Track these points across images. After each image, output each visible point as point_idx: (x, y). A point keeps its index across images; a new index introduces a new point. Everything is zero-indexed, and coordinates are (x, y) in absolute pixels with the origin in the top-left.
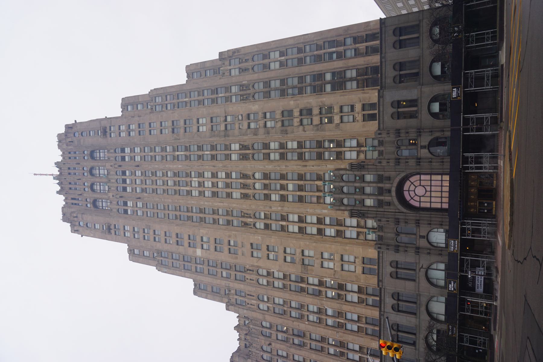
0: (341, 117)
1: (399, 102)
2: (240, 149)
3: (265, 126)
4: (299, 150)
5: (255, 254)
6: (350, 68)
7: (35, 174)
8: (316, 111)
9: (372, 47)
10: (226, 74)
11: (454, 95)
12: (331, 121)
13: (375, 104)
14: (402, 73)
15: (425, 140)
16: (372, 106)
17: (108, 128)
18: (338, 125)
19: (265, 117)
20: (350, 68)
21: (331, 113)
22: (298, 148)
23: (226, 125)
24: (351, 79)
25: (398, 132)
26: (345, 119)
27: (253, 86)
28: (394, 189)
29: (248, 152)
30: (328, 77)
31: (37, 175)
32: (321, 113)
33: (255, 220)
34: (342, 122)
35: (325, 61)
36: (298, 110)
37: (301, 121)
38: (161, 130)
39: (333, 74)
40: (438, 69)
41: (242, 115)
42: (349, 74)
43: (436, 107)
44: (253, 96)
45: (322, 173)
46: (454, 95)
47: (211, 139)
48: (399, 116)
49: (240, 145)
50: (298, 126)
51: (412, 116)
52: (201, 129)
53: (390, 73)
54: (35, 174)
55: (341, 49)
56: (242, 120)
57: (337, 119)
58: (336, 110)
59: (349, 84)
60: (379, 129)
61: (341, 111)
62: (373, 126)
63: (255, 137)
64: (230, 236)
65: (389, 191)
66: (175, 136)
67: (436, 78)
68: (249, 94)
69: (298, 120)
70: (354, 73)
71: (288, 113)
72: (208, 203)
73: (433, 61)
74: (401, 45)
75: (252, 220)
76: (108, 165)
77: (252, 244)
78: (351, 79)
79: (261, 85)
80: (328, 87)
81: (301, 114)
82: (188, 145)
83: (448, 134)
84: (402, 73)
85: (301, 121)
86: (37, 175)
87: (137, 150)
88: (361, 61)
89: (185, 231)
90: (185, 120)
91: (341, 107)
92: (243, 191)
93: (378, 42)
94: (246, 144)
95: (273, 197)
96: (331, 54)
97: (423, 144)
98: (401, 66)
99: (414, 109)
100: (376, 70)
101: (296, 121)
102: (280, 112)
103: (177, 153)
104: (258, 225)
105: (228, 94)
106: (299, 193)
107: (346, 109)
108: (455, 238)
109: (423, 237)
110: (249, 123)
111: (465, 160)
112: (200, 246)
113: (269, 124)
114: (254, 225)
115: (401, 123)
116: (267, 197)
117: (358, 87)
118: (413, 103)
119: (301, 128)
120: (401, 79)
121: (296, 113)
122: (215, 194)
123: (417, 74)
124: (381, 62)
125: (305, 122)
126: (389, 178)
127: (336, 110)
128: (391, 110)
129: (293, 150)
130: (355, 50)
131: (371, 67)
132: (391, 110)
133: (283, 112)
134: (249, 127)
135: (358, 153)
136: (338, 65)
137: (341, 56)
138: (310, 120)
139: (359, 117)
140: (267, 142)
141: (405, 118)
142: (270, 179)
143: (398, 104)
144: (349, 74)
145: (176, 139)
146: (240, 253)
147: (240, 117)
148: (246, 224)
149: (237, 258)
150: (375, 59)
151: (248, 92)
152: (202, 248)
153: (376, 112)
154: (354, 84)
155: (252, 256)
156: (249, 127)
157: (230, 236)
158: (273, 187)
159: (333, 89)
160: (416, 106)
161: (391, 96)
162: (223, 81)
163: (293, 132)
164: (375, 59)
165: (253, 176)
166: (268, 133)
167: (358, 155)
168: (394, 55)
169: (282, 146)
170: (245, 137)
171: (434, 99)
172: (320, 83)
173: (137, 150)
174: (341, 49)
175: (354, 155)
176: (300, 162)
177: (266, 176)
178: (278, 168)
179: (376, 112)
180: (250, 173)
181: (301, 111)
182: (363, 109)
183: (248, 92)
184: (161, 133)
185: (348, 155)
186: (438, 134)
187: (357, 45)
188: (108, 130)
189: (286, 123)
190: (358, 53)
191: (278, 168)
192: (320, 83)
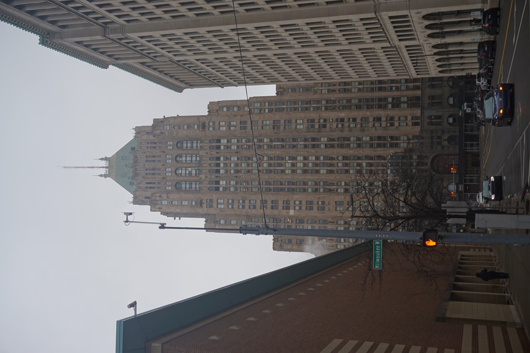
0: (399, 123)
1: (432, 116)
2: (328, 141)
3: (349, 126)
4: (371, 142)
5: (338, 209)
6: (403, 96)
7: (65, 167)
8: (384, 119)
9: (416, 86)
10: (318, 92)
11: (460, 114)
12: (392, 125)
13: (419, 117)
14: (433, 101)
15: (446, 137)
16: (417, 118)
17: (207, 123)
18: (397, 127)
19: (349, 121)
20: (403, 96)
21: (392, 120)
22: (370, 140)
23: (319, 125)
24: (404, 102)
25: (432, 132)
26: (402, 124)
27: (339, 101)
28: (429, 163)
29: (334, 142)
30: (390, 100)
31: (67, 167)
32: (386, 120)
33: (338, 187)
34: (399, 125)
35: (388, 91)
36: (372, 118)
37: (374, 124)
38: (262, 127)
39: (393, 99)
40: (451, 101)
41: (332, 119)
42: (402, 99)
43: (451, 120)
44: (339, 108)
45: (386, 156)
46: (460, 114)
47: (307, 134)
48: (432, 124)
49: (328, 138)
50: (372, 127)
51: (439, 124)
52: (298, 127)
53: (427, 101)
54: (65, 167)
55: (398, 85)
56: (332, 122)
57: (396, 124)
58: (396, 119)
59: (402, 105)
60: (421, 130)
61: (399, 120)
62: (418, 129)
63: (342, 133)
64: (319, 198)
65: (427, 164)
66: (276, 131)
67: (450, 105)
68: (336, 106)
69: (372, 124)
70: (406, 99)
71: (365, 119)
72: (299, 176)
73: (450, 96)
74: (432, 87)
75: (335, 187)
76: (201, 153)
77: (336, 202)
78: (404, 102)
79: (345, 101)
80: (390, 106)
81: (374, 120)
82: (284, 138)
83: (458, 134)
84: (433, 101)
85: (374, 124)
86: (67, 167)
87: (234, 141)
88: (411, 93)
89: (281, 198)
90: (285, 120)
91: (399, 117)
92: (329, 168)
93: (420, 84)
94: (333, 137)
95: (351, 172)
96: (391, 87)
97: (445, 138)
98: (432, 97)
99: (440, 120)
100: (418, 98)
101: (371, 124)
102: (360, 118)
103: (274, 143)
104: (339, 190)
105: (319, 105)
106: (370, 168)
107: (402, 118)
108: (461, 183)
109: (445, 188)
110: (337, 124)
111: (466, 145)
112: (293, 207)
113: (352, 125)
114: (337, 190)
115: (433, 127)
116: (347, 171)
117: (408, 107)
118: (439, 117)
119: (374, 128)
120: (431, 105)
121: (371, 119)
122: (305, 172)
123: (440, 103)
124: (422, 95)
125: (376, 125)
126: (426, 157)
127: (396, 119)
128: (428, 120)
129: (366, 143)
130: (407, 86)
131: (416, 97)
132: (428, 120)
133: (362, 119)
134: (337, 127)
135: (408, 143)
136: (397, 94)
137: (398, 89)
138: (379, 124)
139: (410, 123)
140: (295, 156)
141: (436, 125)
142: (350, 160)
143: (430, 117)
144: (402, 99)
145: (276, 133)
146: (326, 208)
147: (331, 120)
148: (330, 190)
149: (324, 213)
150: (418, 93)
151: (335, 105)
152: (295, 209)
153: (420, 121)
154: (406, 105)
155: (336, 210)
156: (337, 127)
157: (319, 198)
158: (351, 165)
159: (393, 107)
160: (441, 119)
161: (427, 113)
162: (316, 97)
163: (368, 131)
164: (418, 93)
165: (337, 158)
166: (351, 131)
167: (408, 145)
168: (429, 92)
169: (359, 139)
170: (334, 133)
171: (450, 116)
172: (385, 103)
173: (234, 141)
174: (398, 85)
175: (405, 145)
176: (371, 149)
177: (345, 158)
178: (357, 153)
179: (420, 121)
180: (336, 157)
181: (374, 119)
182: (412, 119)
183: (335, 105)
184: (262, 129)
185: (402, 145)
186: (452, 134)
187: (408, 84)
188: (207, 125)
189: (364, 125)
190: (408, 88)
191: (357, 153)
192: (385, 103)
